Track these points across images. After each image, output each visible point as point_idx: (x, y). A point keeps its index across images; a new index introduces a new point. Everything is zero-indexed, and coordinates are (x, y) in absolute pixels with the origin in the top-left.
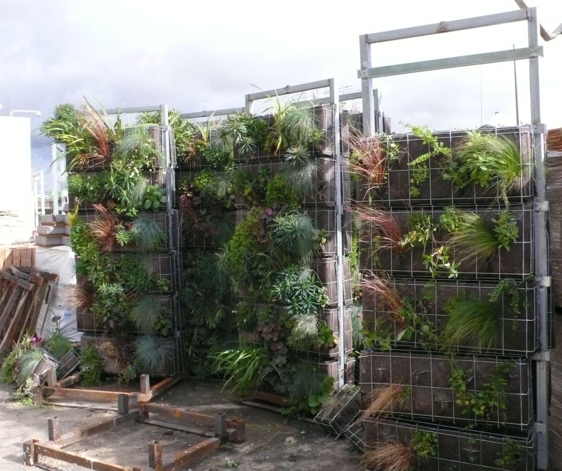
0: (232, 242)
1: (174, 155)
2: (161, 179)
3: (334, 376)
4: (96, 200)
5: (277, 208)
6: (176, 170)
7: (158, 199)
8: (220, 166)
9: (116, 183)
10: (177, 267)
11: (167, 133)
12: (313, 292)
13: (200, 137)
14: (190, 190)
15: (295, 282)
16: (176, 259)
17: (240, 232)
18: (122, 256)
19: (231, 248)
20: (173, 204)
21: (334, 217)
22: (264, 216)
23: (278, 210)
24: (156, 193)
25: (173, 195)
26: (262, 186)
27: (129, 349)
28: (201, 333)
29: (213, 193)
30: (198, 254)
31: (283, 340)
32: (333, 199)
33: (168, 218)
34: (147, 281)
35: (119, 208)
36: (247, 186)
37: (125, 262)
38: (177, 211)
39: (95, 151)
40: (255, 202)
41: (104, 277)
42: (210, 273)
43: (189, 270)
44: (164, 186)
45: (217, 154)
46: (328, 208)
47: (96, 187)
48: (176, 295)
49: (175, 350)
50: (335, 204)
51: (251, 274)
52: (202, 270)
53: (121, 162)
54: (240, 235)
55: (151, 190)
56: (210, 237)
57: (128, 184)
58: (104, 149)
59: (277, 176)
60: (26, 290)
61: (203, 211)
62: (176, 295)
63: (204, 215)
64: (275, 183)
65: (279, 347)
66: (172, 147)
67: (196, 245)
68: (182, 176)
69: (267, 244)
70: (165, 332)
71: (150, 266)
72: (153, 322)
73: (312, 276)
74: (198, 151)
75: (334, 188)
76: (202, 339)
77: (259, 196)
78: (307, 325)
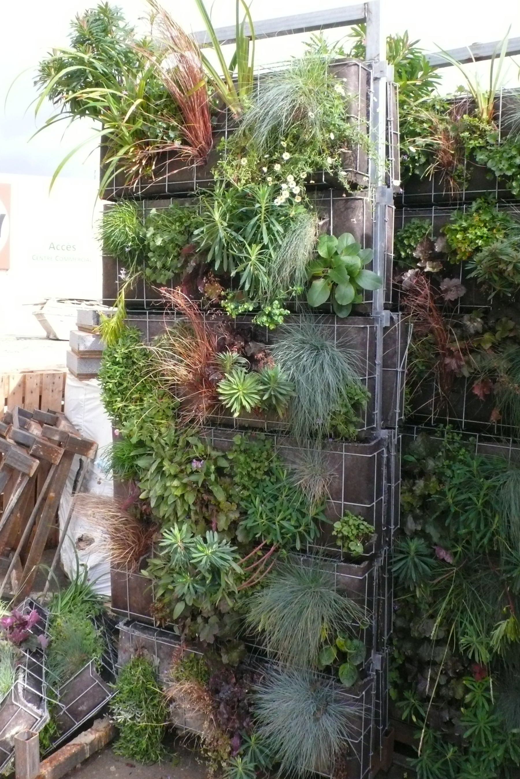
2: (360, 219)
4: (170, 274)
6: (397, 200)
7: (353, 277)
9: (229, 226)
14: (433, 257)
16: (388, 459)
18: (237, 439)
24: (346, 259)
34: (304, 521)
35: (232, 300)
39: (172, 134)
41: (183, 496)
44: (368, 241)
47: (172, 241)
49: (367, 722)
53: (244, 161)
55: (329, 250)
58: (199, 126)
60: (24, 475)
71: (314, 478)
72: (314, 644)
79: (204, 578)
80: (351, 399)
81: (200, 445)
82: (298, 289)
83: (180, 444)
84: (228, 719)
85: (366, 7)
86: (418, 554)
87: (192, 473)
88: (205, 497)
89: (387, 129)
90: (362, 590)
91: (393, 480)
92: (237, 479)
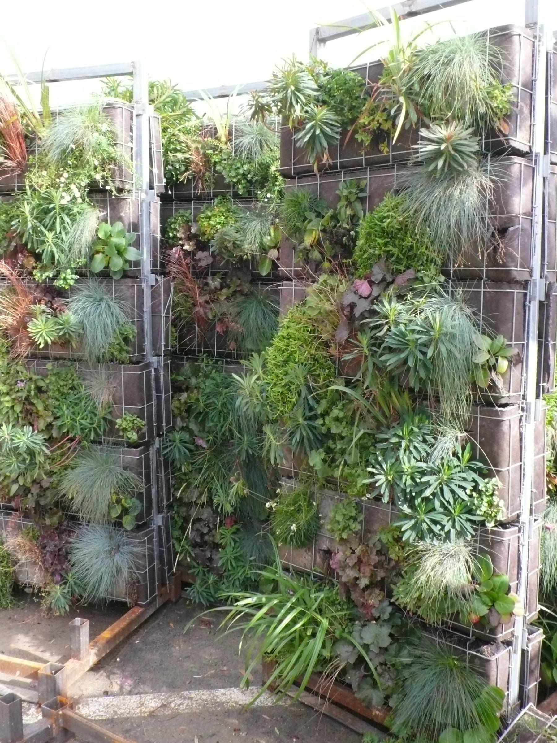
0: (270, 352)
1: (159, 168)
2: (128, 212)
3: (501, 685)
5: (383, 280)
8: (249, 192)
10: (158, 390)
11: (144, 120)
12: (465, 489)
13: (214, 133)
14: (190, 237)
15: (423, 465)
17: (291, 331)
19: (269, 365)
20: (154, 265)
21: (524, 306)
22: (350, 298)
23: (386, 284)
24: (115, 240)
25: (155, 246)
26: (345, 225)
27: (60, 550)
28: (204, 517)
29: (234, 243)
30: (203, 365)
31: (384, 586)
32: (526, 263)
33: (141, 292)
34: (96, 419)
36: (309, 227)
37: (53, 379)
38: (161, 278)
40: (326, 265)
41: (12, 407)
42: (224, 405)
43: (184, 395)
44: (135, 227)
45: (246, 167)
46: (512, 282)
48: (157, 445)
50: (531, 273)
51: (312, 428)
52: (208, 397)
53: (44, 173)
54: (289, 337)
55: (106, 233)
56: (226, 332)
57: (58, 220)
59: (389, 201)
61: (213, 280)
62: (157, 445)
63: (216, 289)
64: (382, 220)
65: (371, 602)
66: (154, 149)
67: (199, 346)
68: (176, 210)
69: (356, 363)
70: (128, 522)
71: (101, 390)
73: (463, 449)
74: (209, 161)
75: (529, 234)
76: (205, 531)
77: (340, 249)
78: (445, 567)
79: (24, 460)
80: (122, 334)
81: (25, 372)
82: (82, 261)
83: (12, 372)
84: (52, 564)
85: (133, 65)
86: (182, 441)
87: (18, 391)
88: (29, 407)
89: (150, 149)
90: (140, 466)
91: (163, 392)
92: (50, 393)
